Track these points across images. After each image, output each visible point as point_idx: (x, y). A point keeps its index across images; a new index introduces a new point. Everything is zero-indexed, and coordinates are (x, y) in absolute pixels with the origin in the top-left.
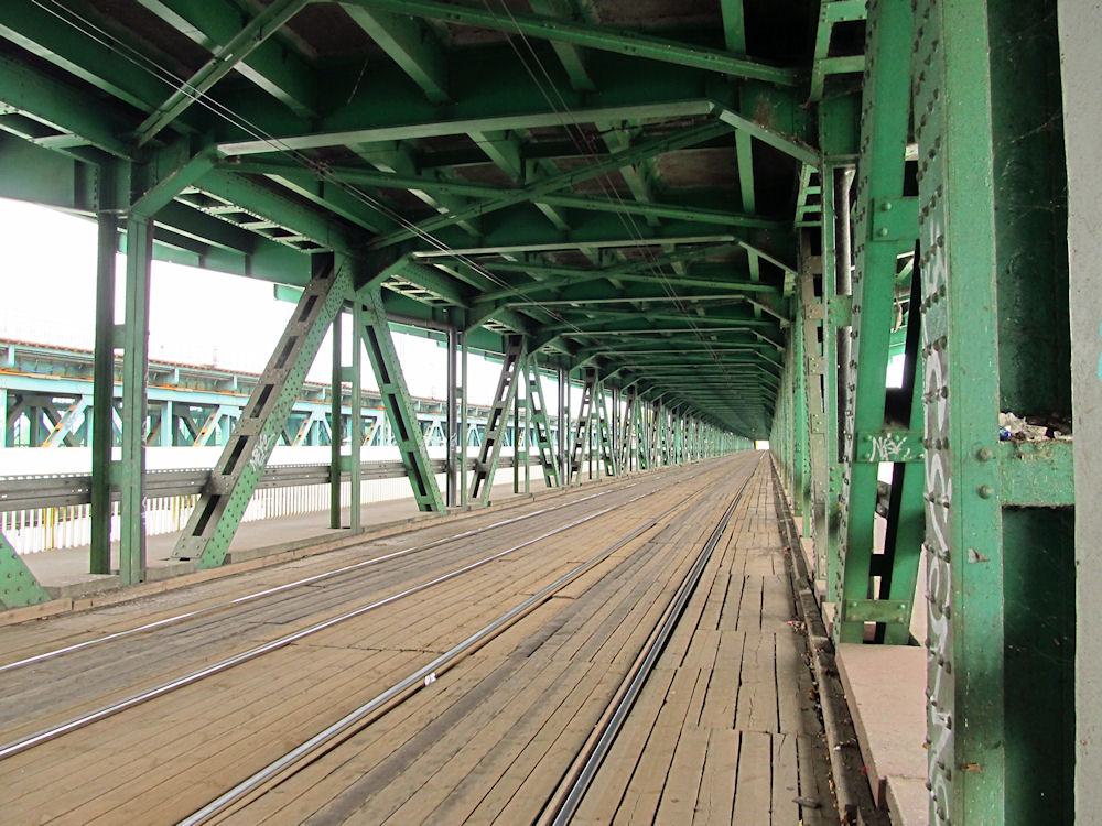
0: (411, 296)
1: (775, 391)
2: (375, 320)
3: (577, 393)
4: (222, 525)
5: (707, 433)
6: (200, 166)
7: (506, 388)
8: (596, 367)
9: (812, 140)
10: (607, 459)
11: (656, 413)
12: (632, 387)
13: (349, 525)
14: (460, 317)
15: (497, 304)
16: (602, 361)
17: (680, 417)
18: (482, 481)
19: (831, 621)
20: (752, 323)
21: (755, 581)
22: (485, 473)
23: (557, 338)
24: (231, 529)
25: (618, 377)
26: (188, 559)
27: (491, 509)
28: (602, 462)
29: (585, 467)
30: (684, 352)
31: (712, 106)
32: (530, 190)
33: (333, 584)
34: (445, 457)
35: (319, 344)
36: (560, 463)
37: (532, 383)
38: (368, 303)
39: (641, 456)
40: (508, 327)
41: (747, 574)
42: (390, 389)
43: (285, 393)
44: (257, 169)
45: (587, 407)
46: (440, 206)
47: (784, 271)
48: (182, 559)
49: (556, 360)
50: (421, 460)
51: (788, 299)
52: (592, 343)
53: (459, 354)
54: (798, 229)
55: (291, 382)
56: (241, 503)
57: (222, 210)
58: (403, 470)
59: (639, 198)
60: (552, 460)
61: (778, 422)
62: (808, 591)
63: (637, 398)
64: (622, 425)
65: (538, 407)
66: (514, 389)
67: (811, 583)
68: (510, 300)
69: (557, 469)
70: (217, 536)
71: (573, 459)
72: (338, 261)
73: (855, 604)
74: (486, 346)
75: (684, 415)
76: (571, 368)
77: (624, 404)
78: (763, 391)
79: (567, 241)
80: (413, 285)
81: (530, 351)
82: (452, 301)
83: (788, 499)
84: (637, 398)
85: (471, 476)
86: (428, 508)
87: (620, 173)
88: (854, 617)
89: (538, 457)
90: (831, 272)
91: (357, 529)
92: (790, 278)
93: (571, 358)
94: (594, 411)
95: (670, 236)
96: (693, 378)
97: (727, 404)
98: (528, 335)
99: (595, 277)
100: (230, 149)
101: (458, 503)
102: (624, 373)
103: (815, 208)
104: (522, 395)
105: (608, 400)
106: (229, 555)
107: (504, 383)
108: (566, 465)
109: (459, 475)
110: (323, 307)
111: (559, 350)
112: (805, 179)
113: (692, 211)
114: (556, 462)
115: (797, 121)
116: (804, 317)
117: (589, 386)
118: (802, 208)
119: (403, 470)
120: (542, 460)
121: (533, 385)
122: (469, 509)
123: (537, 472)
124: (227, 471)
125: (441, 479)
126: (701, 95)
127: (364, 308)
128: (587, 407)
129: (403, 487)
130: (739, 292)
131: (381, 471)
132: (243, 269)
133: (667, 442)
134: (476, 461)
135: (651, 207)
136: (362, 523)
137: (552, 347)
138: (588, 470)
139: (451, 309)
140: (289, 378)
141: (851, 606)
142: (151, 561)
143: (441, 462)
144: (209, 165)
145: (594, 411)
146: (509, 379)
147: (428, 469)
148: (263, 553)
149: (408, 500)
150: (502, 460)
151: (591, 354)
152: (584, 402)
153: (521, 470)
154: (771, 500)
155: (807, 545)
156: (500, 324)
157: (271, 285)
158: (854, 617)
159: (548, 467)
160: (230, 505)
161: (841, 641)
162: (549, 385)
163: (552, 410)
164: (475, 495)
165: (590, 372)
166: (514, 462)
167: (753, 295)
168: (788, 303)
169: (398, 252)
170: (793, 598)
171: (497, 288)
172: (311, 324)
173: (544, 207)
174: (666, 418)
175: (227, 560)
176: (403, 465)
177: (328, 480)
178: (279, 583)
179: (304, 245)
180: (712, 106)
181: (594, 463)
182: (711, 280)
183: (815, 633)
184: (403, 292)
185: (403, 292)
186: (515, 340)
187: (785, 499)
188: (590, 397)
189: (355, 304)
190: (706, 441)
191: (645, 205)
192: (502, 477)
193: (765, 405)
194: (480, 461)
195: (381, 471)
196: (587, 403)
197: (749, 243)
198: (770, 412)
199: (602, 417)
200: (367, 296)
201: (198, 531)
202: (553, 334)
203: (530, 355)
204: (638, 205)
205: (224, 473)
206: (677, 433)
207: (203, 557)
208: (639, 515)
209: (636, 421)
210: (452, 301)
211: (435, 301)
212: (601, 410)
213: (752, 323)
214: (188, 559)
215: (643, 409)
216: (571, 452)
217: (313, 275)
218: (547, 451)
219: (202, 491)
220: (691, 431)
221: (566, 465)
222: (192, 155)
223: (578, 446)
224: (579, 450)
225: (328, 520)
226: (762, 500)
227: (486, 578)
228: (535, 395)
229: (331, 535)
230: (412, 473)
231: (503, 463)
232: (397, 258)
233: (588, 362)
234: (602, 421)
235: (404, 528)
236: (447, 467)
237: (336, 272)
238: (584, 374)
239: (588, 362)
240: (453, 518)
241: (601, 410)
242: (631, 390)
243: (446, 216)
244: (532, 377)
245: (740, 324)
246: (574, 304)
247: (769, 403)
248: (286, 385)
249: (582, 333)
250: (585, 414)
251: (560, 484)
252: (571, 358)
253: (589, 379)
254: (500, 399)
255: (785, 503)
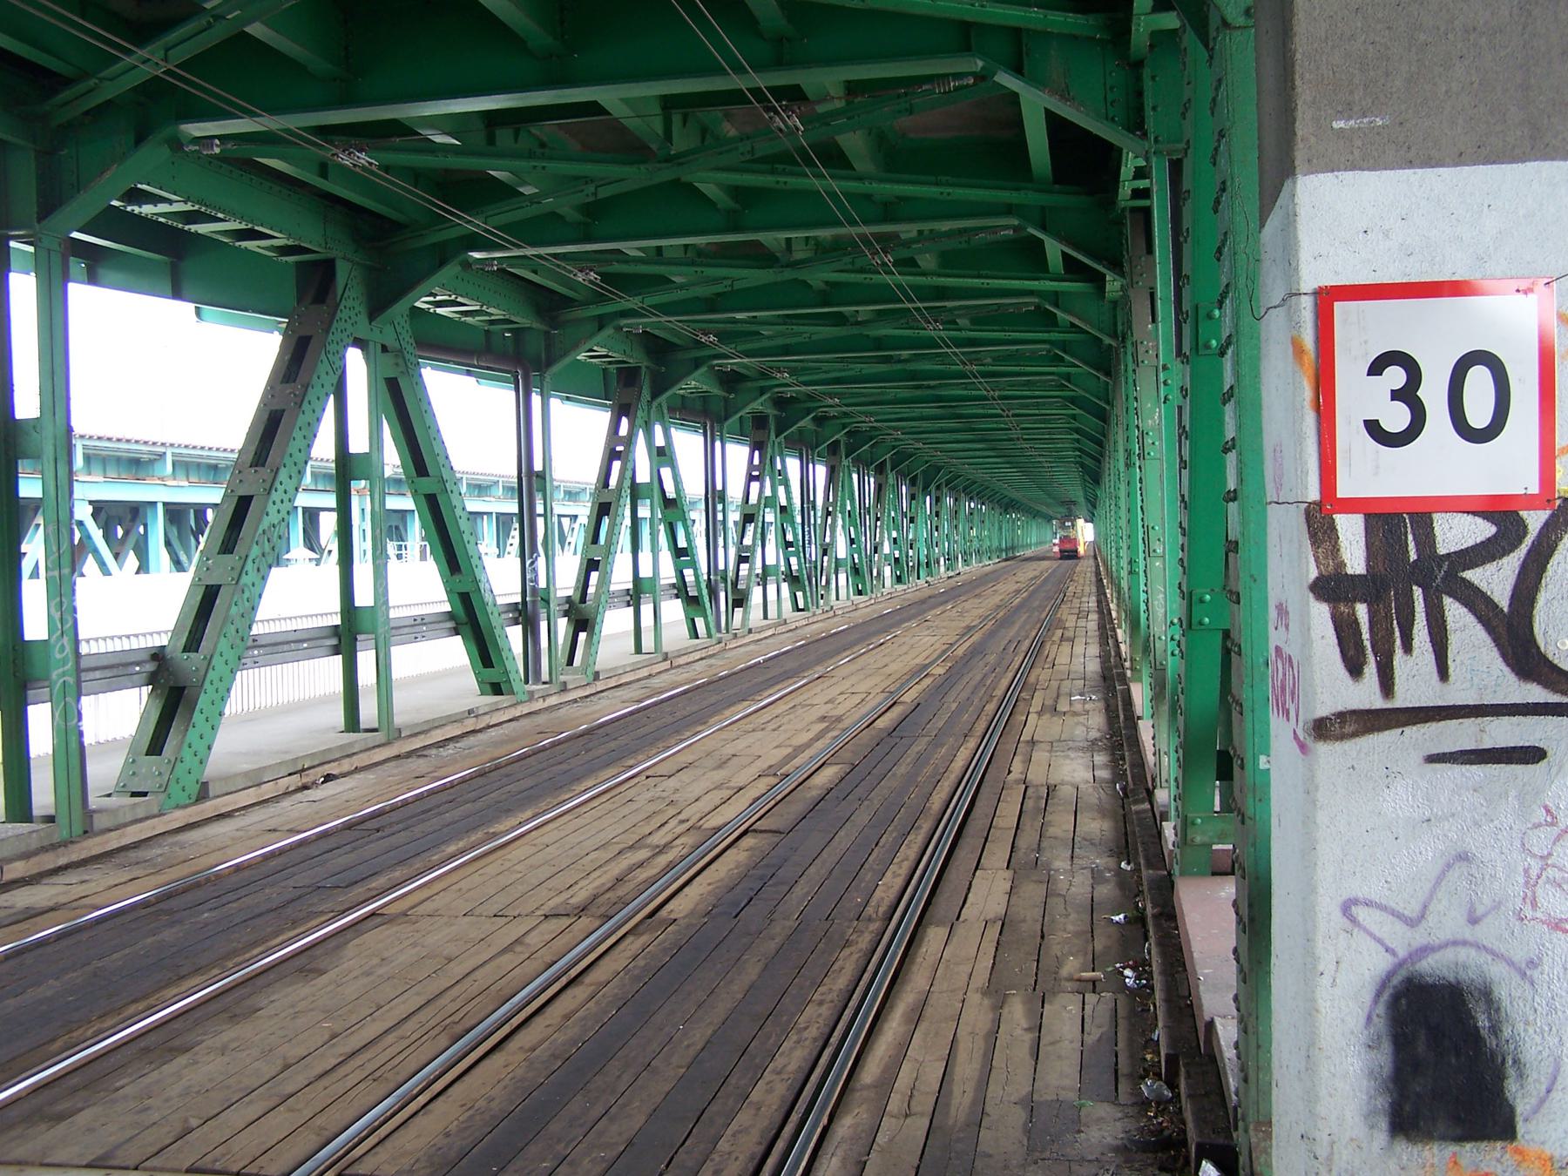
0: (451, 315)
1: (1100, 444)
2: (402, 369)
3: (737, 456)
4: (192, 735)
5: (976, 517)
6: (153, 154)
7: (617, 465)
8: (771, 412)
9: (1136, 125)
10: (793, 580)
11: (879, 488)
12: (836, 444)
13: (376, 725)
14: (534, 345)
15: (601, 322)
16: (780, 402)
17: (926, 490)
18: (582, 636)
19: (1171, 847)
20: (1054, 336)
21: (1066, 792)
22: (586, 621)
23: (704, 369)
24: (205, 742)
25: (811, 426)
26: (145, 794)
27: (600, 686)
28: (785, 587)
29: (756, 594)
30: (932, 383)
31: (980, 64)
32: (681, 164)
33: (391, 825)
34: (518, 599)
35: (319, 420)
36: (713, 593)
37: (661, 452)
38: (390, 341)
39: (856, 571)
40: (618, 356)
41: (1051, 781)
42: (427, 485)
43: (272, 509)
44: (246, 150)
45: (755, 486)
46: (525, 183)
47: (1104, 276)
48: (134, 794)
49: (698, 405)
50: (484, 604)
51: (1115, 303)
52: (764, 375)
53: (718, 444)
54: (1124, 210)
55: (281, 489)
56: (217, 697)
57: (163, 208)
58: (451, 624)
59: (862, 164)
60: (700, 590)
61: (1105, 504)
62: (1146, 806)
63: (845, 462)
64: (819, 514)
65: (671, 493)
66: (630, 466)
67: (1150, 794)
68: (625, 314)
69: (708, 605)
70: (187, 754)
71: (735, 583)
72: (343, 271)
73: (1199, 821)
74: (580, 389)
75: (933, 487)
76: (726, 419)
77: (821, 472)
78: (1078, 441)
79: (736, 229)
80: (460, 299)
81: (655, 394)
82: (523, 321)
83: (1123, 646)
84: (845, 462)
85: (562, 624)
86: (497, 689)
87: (836, 142)
88: (1198, 839)
89: (673, 586)
90: (1165, 284)
91: (389, 730)
92: (1113, 284)
93: (726, 400)
94: (768, 492)
95: (911, 220)
96: (951, 424)
97: (1013, 465)
98: (776, 412)
99: (779, 278)
100: (199, 129)
101: (545, 676)
102: (820, 421)
103: (1142, 184)
104: (643, 476)
105: (793, 465)
106: (205, 785)
107: (611, 455)
108: (722, 595)
109: (543, 626)
110: (323, 357)
111: (705, 388)
112: (1127, 171)
113: (949, 185)
114: (705, 592)
115: (1112, 88)
116: (1136, 362)
117: (758, 446)
118: (1126, 189)
119: (451, 624)
120: (680, 590)
121: (663, 455)
122: (564, 688)
123: (673, 610)
124: (193, 643)
125: (515, 635)
126: (965, 47)
127: (384, 349)
128: (755, 486)
129: (453, 652)
130: (1031, 293)
131: (419, 628)
132: (170, 293)
133: (900, 542)
134: (569, 599)
135: (881, 181)
136: (398, 720)
137: (693, 384)
138: (761, 600)
139: (518, 332)
140: (277, 484)
141: (1193, 824)
142: (94, 802)
143: (513, 607)
144: (165, 152)
145: (768, 492)
146: (620, 448)
147: (496, 620)
148: (255, 779)
149: (461, 670)
150: (613, 595)
151: (762, 391)
152: (751, 478)
153: (647, 610)
154: (1094, 650)
155: (1145, 730)
156: (603, 351)
157: (191, 307)
158: (1198, 839)
159: (692, 602)
160: (203, 702)
161: (1181, 875)
162: (688, 444)
163: (694, 487)
164: (570, 662)
165: (760, 421)
166: (634, 597)
167: (1055, 298)
168: (1115, 308)
169: (442, 255)
170: (1123, 819)
171: (600, 298)
172: (306, 387)
173: (709, 189)
174: (899, 496)
175: (203, 794)
176: (450, 616)
177: (336, 651)
178: (324, 821)
179: (285, 250)
180: (980, 64)
181: (772, 589)
182: (979, 277)
183: (1149, 865)
184: (439, 311)
185: (439, 311)
186: (628, 376)
187: (1117, 644)
188: (761, 467)
189: (371, 345)
190: (974, 533)
191: (871, 179)
192: (615, 622)
193: (1082, 465)
194: (577, 598)
195: (419, 628)
196: (756, 478)
197: (1044, 228)
198: (1093, 476)
199: (784, 502)
200: (389, 329)
201: (156, 747)
202: (697, 363)
203: (655, 404)
204: (860, 179)
205: (186, 649)
206: (919, 520)
207: (170, 790)
208: (862, 687)
209: (843, 505)
210: (523, 321)
211: (492, 322)
212: (781, 490)
213: (1054, 336)
214: (145, 794)
215: (855, 476)
216: (731, 574)
217: (300, 301)
218: (689, 574)
219: (152, 679)
220: (945, 516)
221: (722, 595)
222: (140, 140)
223: (742, 559)
224: (744, 567)
225: (338, 716)
226: (1079, 649)
227: (633, 806)
228: (666, 473)
229: (351, 744)
230: (467, 629)
231: (615, 599)
232: (442, 263)
233: (759, 405)
234: (783, 509)
235: (465, 727)
236: (525, 614)
237: (340, 292)
238: (749, 424)
239: (759, 405)
240: (539, 705)
241: (781, 490)
242: (834, 449)
243: (533, 199)
244: (660, 441)
245: (1038, 339)
246: (631, 248)
247: (1088, 462)
248: (275, 496)
249: (746, 360)
250: (753, 499)
251: (713, 630)
252: (726, 400)
253: (758, 434)
254: (606, 485)
255: (1118, 653)
